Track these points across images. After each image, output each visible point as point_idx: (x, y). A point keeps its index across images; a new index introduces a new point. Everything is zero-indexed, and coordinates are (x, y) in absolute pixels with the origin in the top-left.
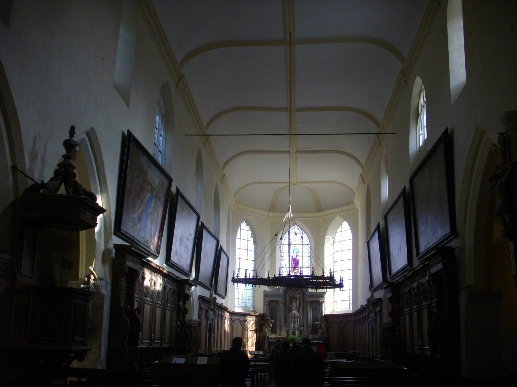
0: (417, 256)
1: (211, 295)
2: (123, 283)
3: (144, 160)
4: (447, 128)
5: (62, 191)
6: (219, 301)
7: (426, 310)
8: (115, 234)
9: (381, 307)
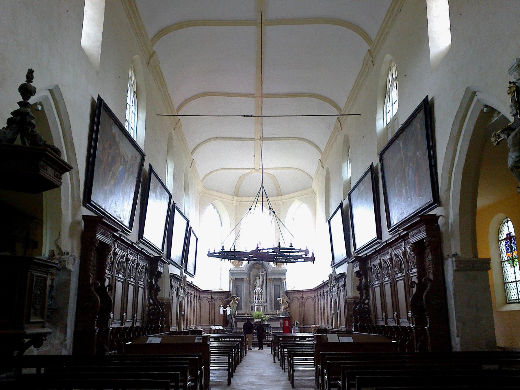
0: (388, 229)
1: (182, 273)
2: (93, 259)
3: (115, 130)
4: (427, 96)
5: (18, 142)
6: (189, 279)
7: (402, 281)
8: (84, 205)
9: (345, 282)
